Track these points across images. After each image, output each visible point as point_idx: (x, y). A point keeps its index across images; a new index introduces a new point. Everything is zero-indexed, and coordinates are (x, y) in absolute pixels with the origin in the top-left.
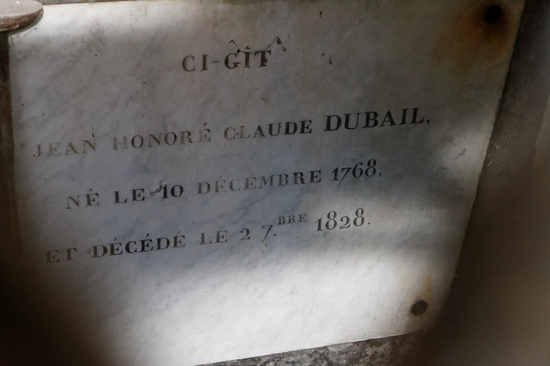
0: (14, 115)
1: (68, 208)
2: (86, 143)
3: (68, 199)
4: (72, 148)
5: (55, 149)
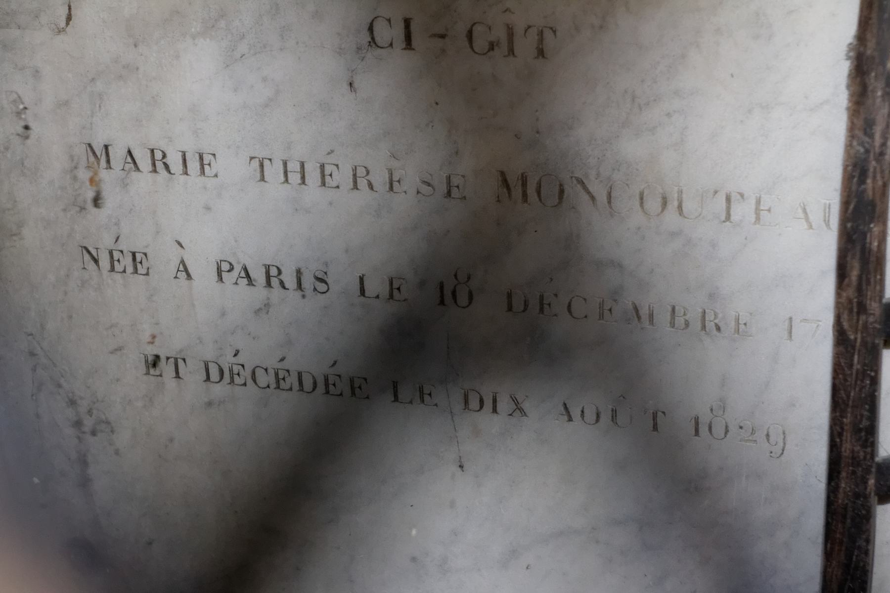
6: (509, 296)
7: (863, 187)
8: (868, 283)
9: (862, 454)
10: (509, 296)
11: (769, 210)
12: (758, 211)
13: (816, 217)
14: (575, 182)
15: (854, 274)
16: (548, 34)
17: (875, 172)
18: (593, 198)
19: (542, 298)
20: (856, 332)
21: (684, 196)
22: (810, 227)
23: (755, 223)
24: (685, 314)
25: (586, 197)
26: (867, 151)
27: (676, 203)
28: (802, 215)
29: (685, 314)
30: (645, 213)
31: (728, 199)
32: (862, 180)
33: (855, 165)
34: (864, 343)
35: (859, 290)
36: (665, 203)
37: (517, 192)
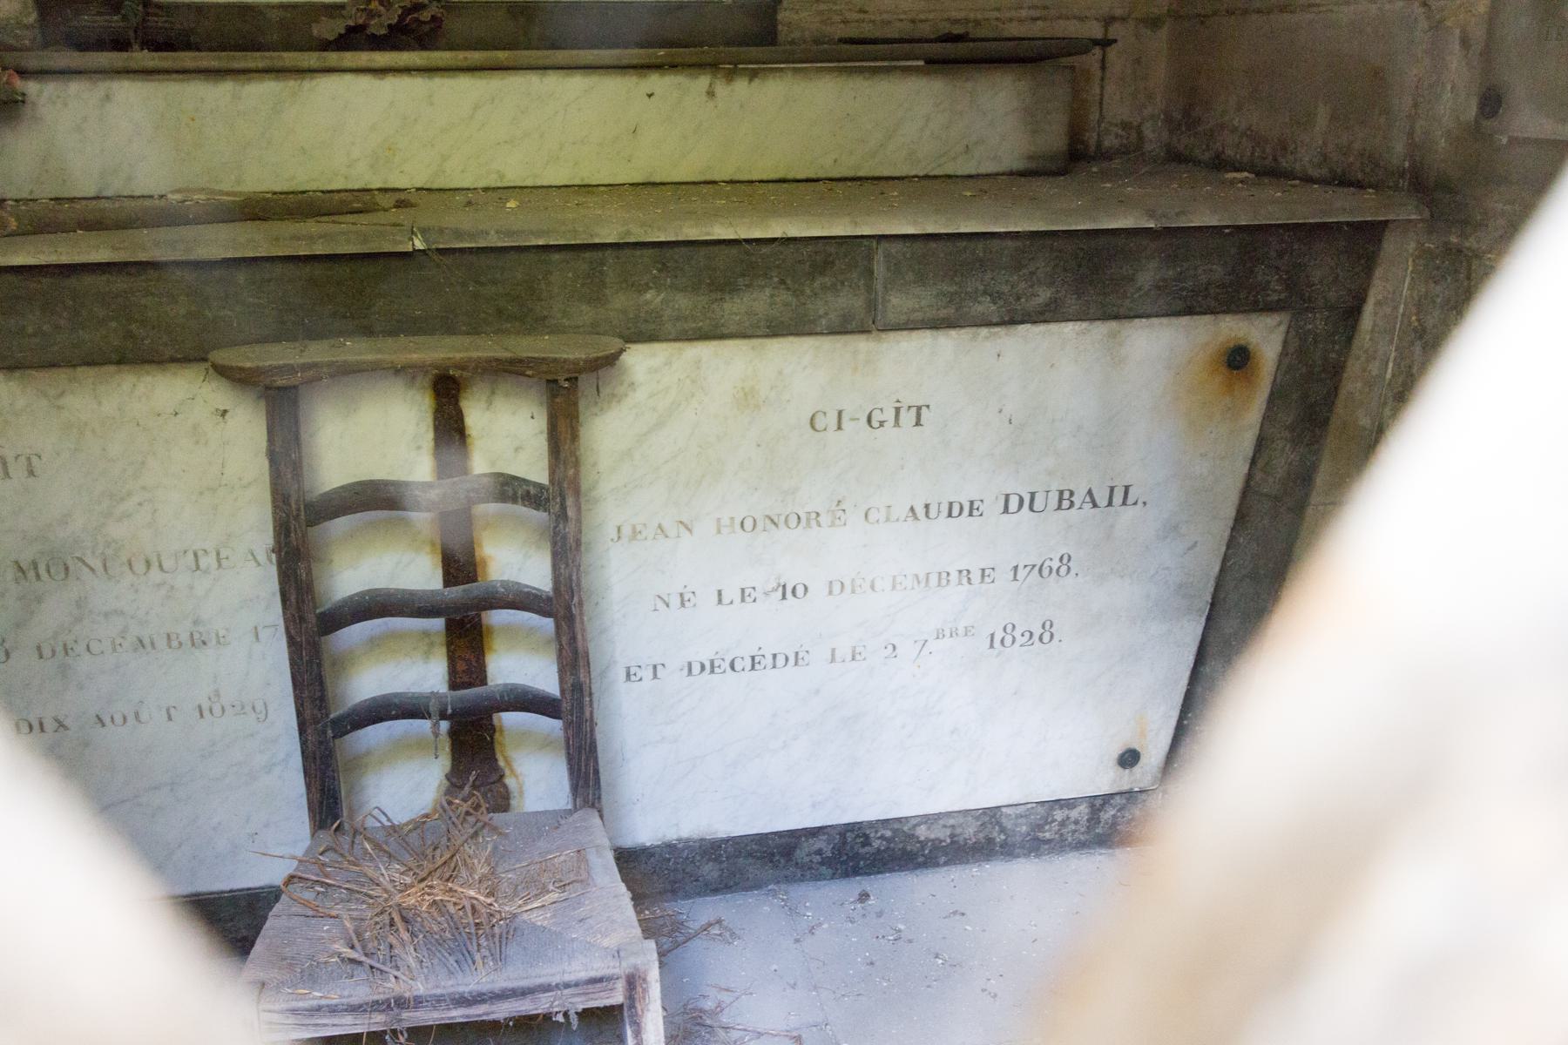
0: (584, 486)
2: (680, 525)
4: (663, 531)
6: (39, 648)
7: (288, 539)
8: (303, 601)
9: (319, 716)
10: (39, 648)
11: (227, 558)
12: (219, 560)
13: (262, 557)
14: (77, 561)
15: (293, 598)
16: (35, 460)
17: (295, 528)
18: (92, 569)
19: (65, 645)
20: (301, 637)
21: (162, 558)
22: (259, 565)
23: (218, 569)
24: (177, 638)
25: (86, 570)
26: (288, 515)
27: (157, 564)
28: (251, 558)
29: (177, 638)
30: (134, 573)
31: (196, 555)
32: (287, 535)
33: (281, 525)
34: (308, 643)
35: (299, 609)
36: (148, 564)
37: (31, 574)
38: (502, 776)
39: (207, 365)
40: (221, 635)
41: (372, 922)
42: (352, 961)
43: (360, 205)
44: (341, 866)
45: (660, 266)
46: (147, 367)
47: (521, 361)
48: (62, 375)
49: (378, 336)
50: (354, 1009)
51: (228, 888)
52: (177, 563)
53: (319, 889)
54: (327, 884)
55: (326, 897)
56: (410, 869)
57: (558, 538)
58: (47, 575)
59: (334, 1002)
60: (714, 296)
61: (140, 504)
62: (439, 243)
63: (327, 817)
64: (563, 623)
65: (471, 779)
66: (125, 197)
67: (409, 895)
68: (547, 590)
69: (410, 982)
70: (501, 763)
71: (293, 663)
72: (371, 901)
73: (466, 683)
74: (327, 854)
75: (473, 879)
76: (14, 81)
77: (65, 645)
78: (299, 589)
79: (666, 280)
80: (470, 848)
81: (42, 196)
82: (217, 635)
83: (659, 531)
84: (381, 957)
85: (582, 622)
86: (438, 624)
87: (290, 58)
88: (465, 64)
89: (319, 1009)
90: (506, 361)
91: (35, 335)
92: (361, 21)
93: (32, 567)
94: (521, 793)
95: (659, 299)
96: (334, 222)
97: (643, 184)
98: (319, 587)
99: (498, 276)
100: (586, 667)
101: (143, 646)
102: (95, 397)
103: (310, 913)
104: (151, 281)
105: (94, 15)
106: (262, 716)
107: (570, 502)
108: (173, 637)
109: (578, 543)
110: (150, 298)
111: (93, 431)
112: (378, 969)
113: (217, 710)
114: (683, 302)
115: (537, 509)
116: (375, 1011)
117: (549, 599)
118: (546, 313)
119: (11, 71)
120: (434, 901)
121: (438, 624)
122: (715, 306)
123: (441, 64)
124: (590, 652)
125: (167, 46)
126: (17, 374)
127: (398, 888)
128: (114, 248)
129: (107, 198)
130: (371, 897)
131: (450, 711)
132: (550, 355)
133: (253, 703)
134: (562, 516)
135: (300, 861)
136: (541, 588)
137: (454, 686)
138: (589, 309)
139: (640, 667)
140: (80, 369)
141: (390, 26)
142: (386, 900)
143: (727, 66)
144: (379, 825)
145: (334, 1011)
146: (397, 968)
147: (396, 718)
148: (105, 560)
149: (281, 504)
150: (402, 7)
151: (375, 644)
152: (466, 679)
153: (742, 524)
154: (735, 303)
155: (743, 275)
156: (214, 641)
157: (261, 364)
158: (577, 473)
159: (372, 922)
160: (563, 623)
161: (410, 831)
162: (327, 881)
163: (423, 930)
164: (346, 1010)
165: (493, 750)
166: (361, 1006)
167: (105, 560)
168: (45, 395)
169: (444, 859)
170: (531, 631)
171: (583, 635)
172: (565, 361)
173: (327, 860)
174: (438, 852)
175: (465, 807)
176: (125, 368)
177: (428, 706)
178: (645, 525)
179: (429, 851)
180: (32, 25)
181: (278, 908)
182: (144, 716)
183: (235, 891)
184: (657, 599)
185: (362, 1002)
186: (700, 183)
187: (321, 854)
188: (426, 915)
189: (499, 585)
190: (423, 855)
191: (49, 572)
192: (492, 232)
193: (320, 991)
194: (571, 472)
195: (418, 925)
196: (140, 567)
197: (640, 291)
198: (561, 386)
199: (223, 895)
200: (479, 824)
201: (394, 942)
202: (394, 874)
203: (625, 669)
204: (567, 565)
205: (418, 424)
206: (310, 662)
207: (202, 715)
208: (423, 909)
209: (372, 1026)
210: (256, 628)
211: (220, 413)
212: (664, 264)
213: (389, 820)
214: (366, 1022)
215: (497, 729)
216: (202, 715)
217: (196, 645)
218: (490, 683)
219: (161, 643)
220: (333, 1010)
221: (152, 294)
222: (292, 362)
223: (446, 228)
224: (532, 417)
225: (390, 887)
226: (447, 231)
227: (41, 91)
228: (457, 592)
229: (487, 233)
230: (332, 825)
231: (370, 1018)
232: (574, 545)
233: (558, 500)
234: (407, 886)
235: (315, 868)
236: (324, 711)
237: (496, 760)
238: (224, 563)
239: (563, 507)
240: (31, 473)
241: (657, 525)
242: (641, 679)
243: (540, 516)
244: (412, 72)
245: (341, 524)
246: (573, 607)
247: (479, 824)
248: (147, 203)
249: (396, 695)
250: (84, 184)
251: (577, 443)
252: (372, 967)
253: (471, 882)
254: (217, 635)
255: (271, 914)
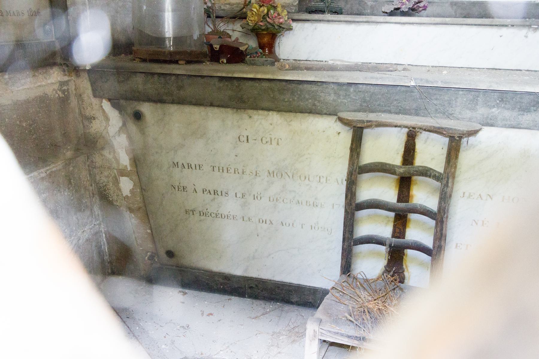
0: (456, 175)
1: (478, 220)
2: (488, 196)
3: (116, 133)
4: (481, 197)
5: (472, 196)
12: (326, 180)
18: (289, 177)
19: (277, 198)
25: (287, 176)
26: (353, 169)
28: (337, 181)
31: (320, 177)
32: (351, 176)
34: (351, 212)
35: (350, 200)
37: (272, 175)
38: (404, 271)
39: (336, 117)
40: (322, 204)
41: (357, 309)
42: (350, 321)
43: (392, 69)
44: (349, 288)
45: (500, 99)
46: (317, 115)
47: (442, 128)
48: (292, 114)
49: (392, 114)
50: (349, 337)
51: (309, 285)
52: (314, 178)
53: (341, 293)
54: (343, 293)
55: (343, 297)
56: (371, 295)
57: (444, 193)
58: (276, 176)
59: (343, 332)
60: (520, 112)
61: (307, 159)
62: (420, 84)
63: (346, 271)
64: (439, 223)
65: (394, 269)
66: (315, 61)
67: (370, 304)
68: (436, 210)
69: (368, 333)
70: (404, 267)
71: (345, 218)
72: (357, 302)
73: (398, 236)
74: (344, 283)
75: (392, 304)
76: (291, 22)
77: (277, 198)
78: (352, 194)
79: (501, 105)
80: (392, 293)
81: (291, 59)
82: (321, 204)
83: (479, 197)
84: (359, 322)
85: (446, 224)
86: (392, 214)
87: (374, 18)
88: (434, 22)
89: (338, 333)
90: (437, 128)
91: (287, 102)
92: (399, 7)
93: (272, 173)
94: (409, 278)
95: (497, 112)
96: (384, 74)
97: (492, 69)
98: (357, 194)
99: (439, 97)
100: (444, 241)
101: (299, 203)
102: (300, 123)
103: (338, 301)
104: (324, 88)
105: (316, 2)
106: (330, 233)
107: (450, 181)
108: (308, 202)
109: (450, 196)
110: (323, 94)
111: (298, 133)
112: (358, 326)
113: (316, 228)
114: (507, 114)
115: (438, 181)
116: (355, 339)
117: (435, 214)
118: (453, 112)
119: (290, 19)
120: (379, 308)
121: (392, 214)
122: (519, 117)
123: (425, 22)
124: (447, 235)
125: (336, 13)
126: (280, 113)
127: (366, 300)
128: (316, 77)
129: (309, 61)
130: (357, 301)
131: (393, 245)
132: (453, 127)
133: (328, 228)
134: (447, 185)
135: (336, 283)
136: (433, 209)
137: (393, 236)
138: (470, 112)
139: (461, 244)
140: (298, 114)
141: (409, 8)
142: (362, 303)
143: (535, 26)
144: (362, 277)
145: (342, 335)
146: (365, 327)
147: (374, 243)
148: (293, 174)
149: (351, 165)
150: (414, 2)
151: (369, 216)
152: (398, 235)
153: (513, 200)
154: (528, 116)
155: (534, 106)
156: (320, 206)
157: (354, 119)
158: (455, 172)
159: (357, 309)
160: (439, 223)
161: (372, 282)
162: (344, 292)
163: (374, 317)
164: (346, 336)
165: (402, 261)
166: (351, 337)
167: (293, 174)
168: (286, 120)
169: (383, 295)
170: (424, 223)
171: (445, 229)
172: (459, 130)
173: (344, 285)
174: (381, 292)
175: (392, 279)
176: (310, 114)
177: (386, 242)
178: (474, 193)
179: (378, 291)
180: (296, 5)
181: (327, 296)
182: (295, 225)
183: (311, 287)
184: (473, 221)
185: (351, 335)
186: (514, 70)
187: (343, 282)
188: (375, 312)
189: (418, 205)
190: (376, 291)
191: (277, 175)
192: (440, 82)
193: (339, 327)
194: (453, 170)
195: (373, 315)
196: (303, 178)
197: (490, 108)
198: (456, 139)
199: (307, 287)
200: (395, 286)
201: (365, 318)
202: (366, 295)
203: (456, 244)
204: (445, 203)
205: (399, 145)
206: (351, 219)
207: (312, 228)
208: (375, 310)
209: (353, 344)
210: (333, 204)
211: (338, 133)
212: (502, 99)
213: (366, 277)
214: (352, 342)
215: (405, 255)
216: (312, 228)
217: (315, 206)
218: (406, 238)
219: (304, 203)
220: (342, 335)
221: (324, 92)
222: (364, 119)
223: (423, 79)
224: (442, 149)
225: (364, 299)
226: (423, 80)
227: (297, 26)
228: (402, 205)
229: (438, 82)
230: (347, 274)
231: (353, 341)
232: (448, 196)
233: (446, 179)
234: (370, 301)
235: (341, 287)
236: (352, 236)
237: (403, 265)
238: (328, 181)
239: (447, 182)
240: (278, 144)
241: (479, 195)
242: (461, 249)
243: (438, 184)
244: (414, 24)
245: (366, 176)
246: (444, 218)
247: (395, 286)
248: (322, 63)
249: (376, 236)
250: (303, 56)
251: (457, 160)
252: (356, 325)
253: (391, 305)
254: (321, 204)
255: (325, 298)
